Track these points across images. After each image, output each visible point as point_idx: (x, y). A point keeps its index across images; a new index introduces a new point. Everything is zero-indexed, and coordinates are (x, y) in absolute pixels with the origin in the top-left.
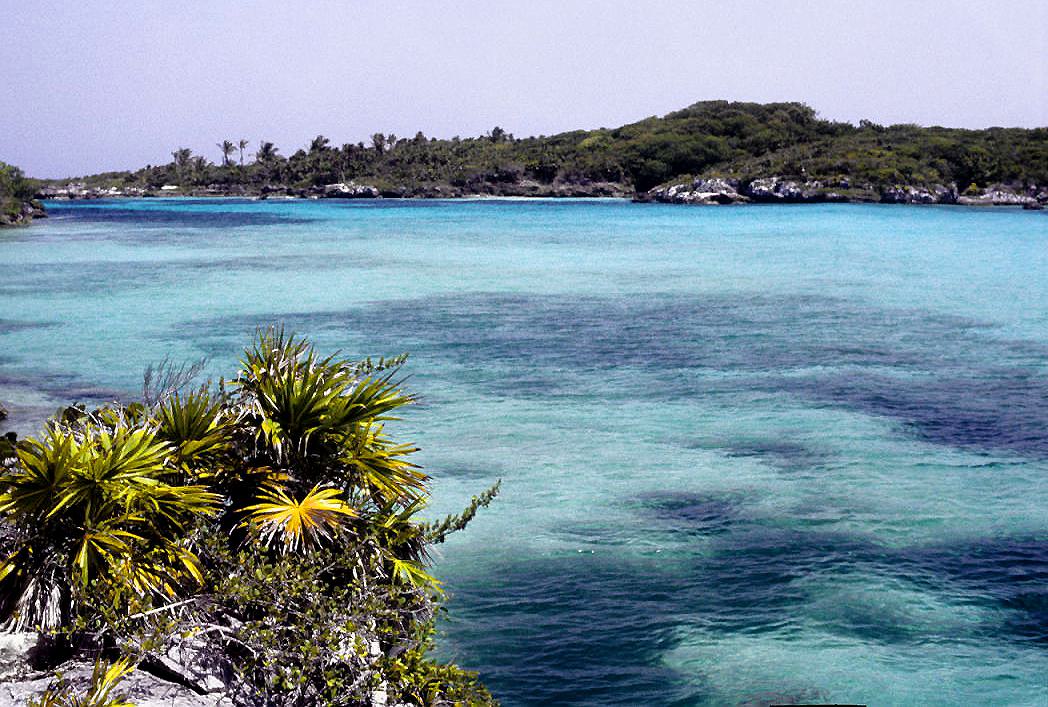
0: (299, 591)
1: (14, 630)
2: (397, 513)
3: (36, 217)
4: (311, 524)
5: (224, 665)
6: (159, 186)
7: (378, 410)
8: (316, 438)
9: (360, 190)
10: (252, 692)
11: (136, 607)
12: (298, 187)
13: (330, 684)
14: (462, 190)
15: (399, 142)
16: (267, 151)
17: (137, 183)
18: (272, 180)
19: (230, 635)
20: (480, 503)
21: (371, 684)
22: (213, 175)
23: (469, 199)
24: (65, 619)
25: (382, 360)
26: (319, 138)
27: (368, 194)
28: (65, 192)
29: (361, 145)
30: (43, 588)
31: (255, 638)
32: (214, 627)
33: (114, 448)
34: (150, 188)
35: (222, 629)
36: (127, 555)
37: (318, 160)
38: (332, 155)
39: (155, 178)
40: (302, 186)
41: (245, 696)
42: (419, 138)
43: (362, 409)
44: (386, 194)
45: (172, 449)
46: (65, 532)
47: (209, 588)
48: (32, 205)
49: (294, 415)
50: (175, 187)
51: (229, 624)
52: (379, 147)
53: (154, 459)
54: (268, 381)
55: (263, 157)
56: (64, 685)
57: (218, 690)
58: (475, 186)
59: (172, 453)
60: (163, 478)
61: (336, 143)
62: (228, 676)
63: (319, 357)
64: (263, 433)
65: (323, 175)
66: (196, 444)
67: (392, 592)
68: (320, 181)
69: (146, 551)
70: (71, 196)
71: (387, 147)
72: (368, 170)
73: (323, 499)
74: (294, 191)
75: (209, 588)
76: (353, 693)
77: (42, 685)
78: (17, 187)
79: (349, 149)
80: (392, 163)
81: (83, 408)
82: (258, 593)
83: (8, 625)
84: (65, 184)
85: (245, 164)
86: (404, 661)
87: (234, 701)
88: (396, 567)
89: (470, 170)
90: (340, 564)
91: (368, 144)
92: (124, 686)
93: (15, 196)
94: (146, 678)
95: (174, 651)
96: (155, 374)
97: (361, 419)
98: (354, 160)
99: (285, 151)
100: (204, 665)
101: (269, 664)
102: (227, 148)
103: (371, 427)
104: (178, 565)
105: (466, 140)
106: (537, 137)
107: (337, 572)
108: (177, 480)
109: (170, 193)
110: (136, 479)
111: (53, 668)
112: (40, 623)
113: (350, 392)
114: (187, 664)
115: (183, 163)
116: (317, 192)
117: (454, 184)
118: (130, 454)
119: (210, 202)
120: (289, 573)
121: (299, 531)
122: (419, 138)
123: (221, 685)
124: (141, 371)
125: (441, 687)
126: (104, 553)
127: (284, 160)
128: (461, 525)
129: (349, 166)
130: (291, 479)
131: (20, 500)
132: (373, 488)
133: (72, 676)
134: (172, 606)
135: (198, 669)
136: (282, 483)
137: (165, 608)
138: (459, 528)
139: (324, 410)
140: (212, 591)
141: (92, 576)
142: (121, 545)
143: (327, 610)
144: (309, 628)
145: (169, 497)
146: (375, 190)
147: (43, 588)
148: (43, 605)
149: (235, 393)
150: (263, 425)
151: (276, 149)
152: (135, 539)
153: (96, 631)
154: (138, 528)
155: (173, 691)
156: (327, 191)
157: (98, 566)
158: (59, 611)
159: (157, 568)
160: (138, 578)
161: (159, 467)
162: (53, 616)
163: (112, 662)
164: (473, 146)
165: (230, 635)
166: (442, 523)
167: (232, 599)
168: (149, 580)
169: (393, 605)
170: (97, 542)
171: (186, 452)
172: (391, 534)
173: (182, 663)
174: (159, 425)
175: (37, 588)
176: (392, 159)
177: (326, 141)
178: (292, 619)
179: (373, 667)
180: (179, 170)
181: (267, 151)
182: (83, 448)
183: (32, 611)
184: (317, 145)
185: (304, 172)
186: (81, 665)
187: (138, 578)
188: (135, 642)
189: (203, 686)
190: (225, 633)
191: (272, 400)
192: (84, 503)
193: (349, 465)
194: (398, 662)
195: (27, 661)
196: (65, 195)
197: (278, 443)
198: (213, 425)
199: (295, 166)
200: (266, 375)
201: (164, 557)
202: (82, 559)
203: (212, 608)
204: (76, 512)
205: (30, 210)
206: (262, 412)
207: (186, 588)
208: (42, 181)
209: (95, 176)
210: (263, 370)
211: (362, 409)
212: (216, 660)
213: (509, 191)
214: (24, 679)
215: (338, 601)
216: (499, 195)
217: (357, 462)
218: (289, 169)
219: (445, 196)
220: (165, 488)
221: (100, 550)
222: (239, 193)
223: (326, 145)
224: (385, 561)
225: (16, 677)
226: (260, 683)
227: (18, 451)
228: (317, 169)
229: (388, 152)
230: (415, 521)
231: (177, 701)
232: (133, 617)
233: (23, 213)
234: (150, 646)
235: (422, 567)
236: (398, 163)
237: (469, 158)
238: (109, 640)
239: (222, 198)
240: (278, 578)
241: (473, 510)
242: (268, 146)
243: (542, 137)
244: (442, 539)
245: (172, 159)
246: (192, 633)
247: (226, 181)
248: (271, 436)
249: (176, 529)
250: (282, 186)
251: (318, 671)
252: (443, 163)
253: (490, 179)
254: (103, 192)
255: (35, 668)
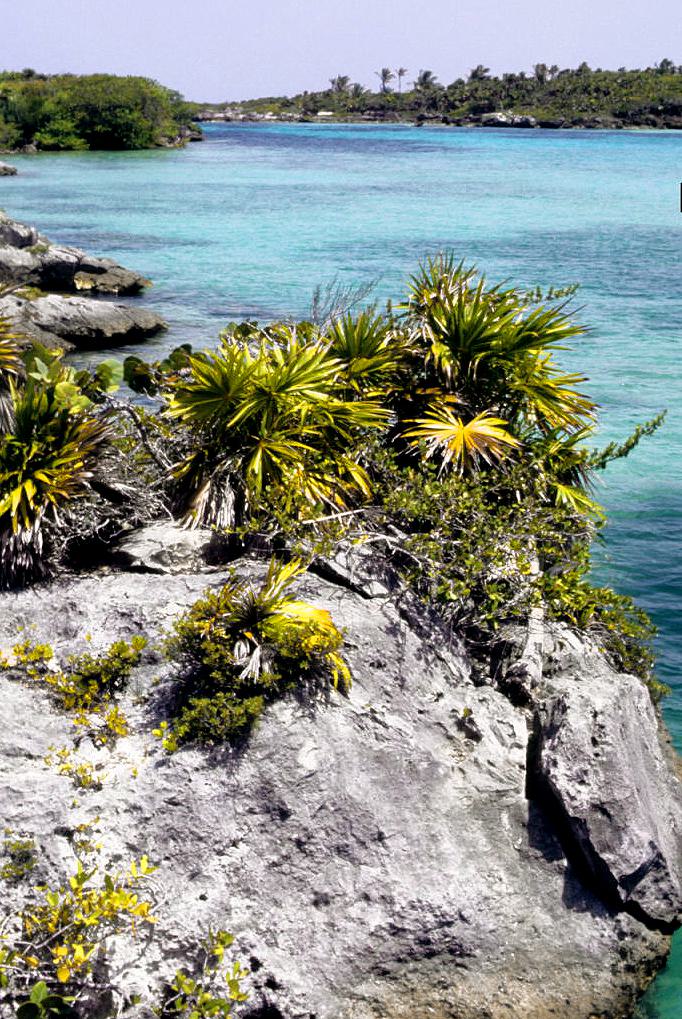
0: (467, 508)
1: (190, 526)
2: (563, 440)
3: (193, 140)
4: (473, 447)
5: (388, 572)
6: (315, 112)
7: (547, 339)
8: (484, 364)
9: (517, 119)
10: (415, 599)
11: (307, 513)
12: (454, 115)
13: (493, 597)
14: (624, 123)
15: (562, 73)
16: (425, 79)
17: (293, 107)
18: (428, 108)
19: (396, 544)
20: (643, 432)
21: (530, 599)
22: (370, 102)
23: (390, 136)
24: (238, 520)
25: (552, 289)
26: (480, 67)
27: (525, 124)
28: (222, 115)
29: (522, 75)
30: (219, 491)
31: (427, 552)
32: (381, 536)
33: (287, 364)
34: (305, 113)
35: (389, 539)
36: (299, 465)
37: (476, 90)
38: (491, 84)
39: (310, 105)
40: (459, 114)
41: (407, 603)
42: (583, 69)
43: (532, 336)
44: (545, 125)
45: (343, 366)
46: (243, 441)
47: (378, 500)
48: (189, 128)
49: (463, 341)
50: (330, 113)
51: (395, 535)
52: (541, 78)
53: (326, 374)
54: (438, 305)
55: (421, 84)
56: (234, 580)
57: (382, 596)
58: (637, 119)
59: (343, 370)
60: (335, 393)
61: (497, 72)
62: (392, 583)
63: (488, 285)
64: (433, 355)
65: (477, 104)
66: (364, 362)
67: (556, 516)
68: (477, 110)
69: (318, 462)
70: (228, 120)
71: (549, 78)
72: (528, 99)
73: (485, 426)
74: (450, 118)
75: (378, 500)
76: (511, 608)
77: (215, 578)
78: (178, 111)
79: (510, 79)
80: (553, 94)
81: (255, 324)
82: (425, 507)
83: (184, 523)
84: (222, 108)
85: (403, 91)
86: (564, 581)
87: (397, 606)
88: (559, 494)
89: (633, 101)
90: (506, 485)
91: (530, 74)
92: (294, 586)
93: (175, 118)
94: (314, 579)
95: (342, 555)
96: (324, 295)
97: (532, 347)
98: (514, 90)
99: (444, 79)
100: (369, 571)
101: (432, 575)
102: (385, 75)
103: (539, 355)
104: (347, 477)
105: (633, 72)
106: (643, 69)
107: (503, 492)
108: (349, 395)
109: (325, 119)
110: (307, 392)
111: (225, 563)
112: (215, 522)
113: (518, 320)
114: (353, 569)
115: (340, 90)
116: (472, 121)
117: (615, 115)
118: (304, 367)
119: (364, 130)
120: (457, 491)
121: (460, 449)
122: (583, 69)
123: (385, 591)
124: (311, 291)
125: (596, 609)
126: (278, 461)
127: (442, 89)
128: (623, 453)
129: (509, 96)
130: (459, 401)
131: (197, 406)
132: (540, 415)
133: (246, 573)
134: (339, 516)
135: (364, 575)
136: (448, 404)
137: (334, 516)
138: (621, 455)
139: (493, 337)
140: (382, 503)
141: (265, 483)
142: (295, 455)
143: (492, 528)
144: (473, 543)
145: (343, 411)
146: (533, 120)
147: (219, 491)
148: (218, 506)
149: (403, 316)
150: (433, 347)
151: (435, 78)
152: (308, 451)
153: (269, 532)
154: (311, 441)
155: (339, 593)
156: (484, 120)
157: (272, 473)
158: (233, 512)
159: (327, 478)
160: (310, 488)
161: (330, 383)
162: (226, 517)
163: (285, 563)
164: (639, 77)
165: (396, 544)
166: (602, 450)
167: (400, 513)
168: (320, 489)
169: (559, 527)
170: (272, 451)
171: (355, 369)
172: (556, 459)
173: (349, 568)
174: (330, 344)
175: (213, 491)
176: (552, 89)
177: (486, 70)
178: (457, 535)
179: (533, 585)
180: (335, 97)
181: (425, 79)
182: (256, 361)
183: (208, 510)
184: (477, 75)
185: (461, 101)
186: (252, 563)
187: (310, 488)
188: (305, 545)
189: (368, 591)
190: (392, 543)
191: (442, 324)
192: (259, 415)
193: (517, 391)
194: (559, 582)
195: (201, 556)
196: (221, 118)
197: (447, 366)
198: (383, 345)
199: (453, 94)
200: (436, 299)
201: (335, 467)
202: (257, 465)
203: (381, 519)
204: (252, 424)
205: (188, 132)
206: (432, 337)
207: (354, 500)
208: (201, 105)
209: (251, 102)
210: (434, 295)
211: (532, 336)
212: (381, 567)
213: (673, 124)
214: (198, 572)
215: (503, 520)
216: (662, 128)
217: (525, 388)
218: (446, 97)
219: (606, 127)
220: (337, 403)
221: (274, 459)
222: (394, 119)
223: (486, 74)
224: (549, 486)
225: (191, 570)
226: (425, 592)
227: (192, 360)
228: (475, 98)
229: (549, 83)
230: (577, 448)
231: (343, 602)
232: (305, 522)
233: (181, 136)
234: (322, 550)
235: (584, 494)
236: (559, 94)
237: (634, 89)
238: (279, 542)
239: (377, 124)
240: (446, 494)
241: (637, 439)
242: (427, 75)
243: (599, 71)
244: (603, 465)
245: (330, 86)
246: (360, 541)
247: (382, 108)
248: (440, 358)
249: (345, 442)
250: (438, 114)
251: (479, 586)
252: (606, 94)
253: (654, 111)
254: (259, 116)
255: (208, 563)
